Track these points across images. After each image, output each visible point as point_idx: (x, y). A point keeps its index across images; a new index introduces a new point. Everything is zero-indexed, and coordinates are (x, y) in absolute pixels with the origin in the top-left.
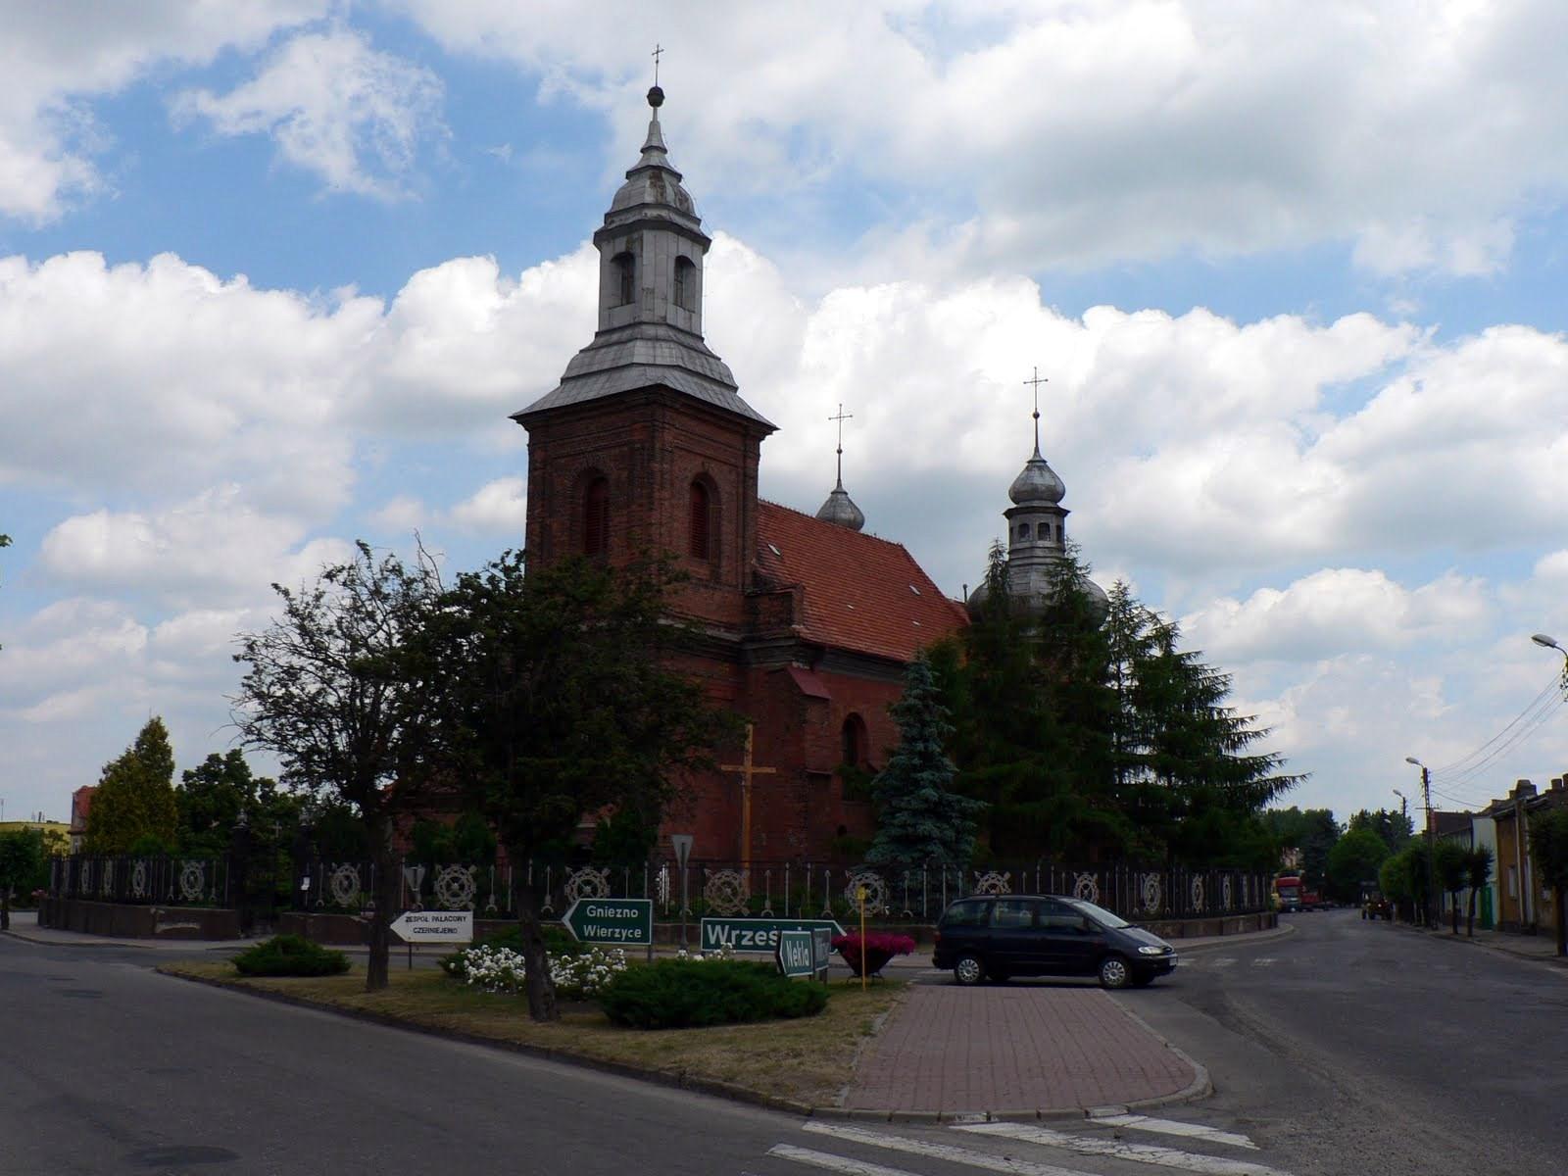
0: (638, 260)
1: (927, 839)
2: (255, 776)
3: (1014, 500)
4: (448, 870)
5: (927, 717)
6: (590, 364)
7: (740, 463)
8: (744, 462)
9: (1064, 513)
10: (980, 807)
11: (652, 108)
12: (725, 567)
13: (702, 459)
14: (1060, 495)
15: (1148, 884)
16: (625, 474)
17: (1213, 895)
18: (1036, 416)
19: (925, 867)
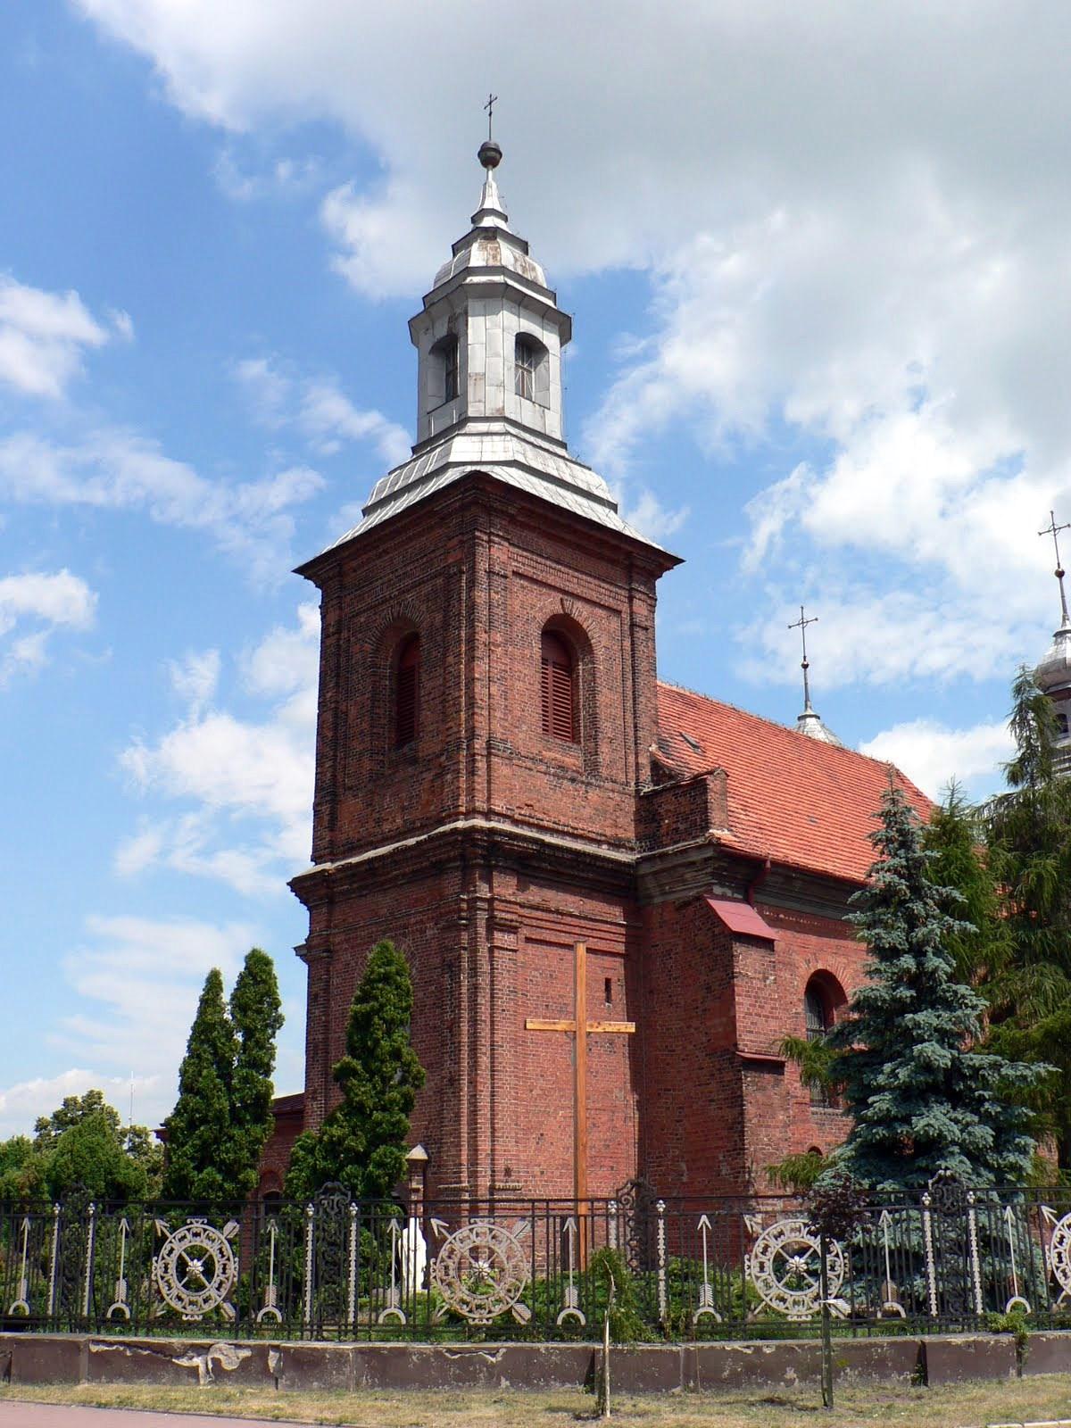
1: (932, 1146)
2: (124, 1124)
5: (918, 907)
7: (625, 608)
8: (631, 607)
10: (1038, 1074)
12: (605, 753)
16: (439, 617)
19: (927, 1199)
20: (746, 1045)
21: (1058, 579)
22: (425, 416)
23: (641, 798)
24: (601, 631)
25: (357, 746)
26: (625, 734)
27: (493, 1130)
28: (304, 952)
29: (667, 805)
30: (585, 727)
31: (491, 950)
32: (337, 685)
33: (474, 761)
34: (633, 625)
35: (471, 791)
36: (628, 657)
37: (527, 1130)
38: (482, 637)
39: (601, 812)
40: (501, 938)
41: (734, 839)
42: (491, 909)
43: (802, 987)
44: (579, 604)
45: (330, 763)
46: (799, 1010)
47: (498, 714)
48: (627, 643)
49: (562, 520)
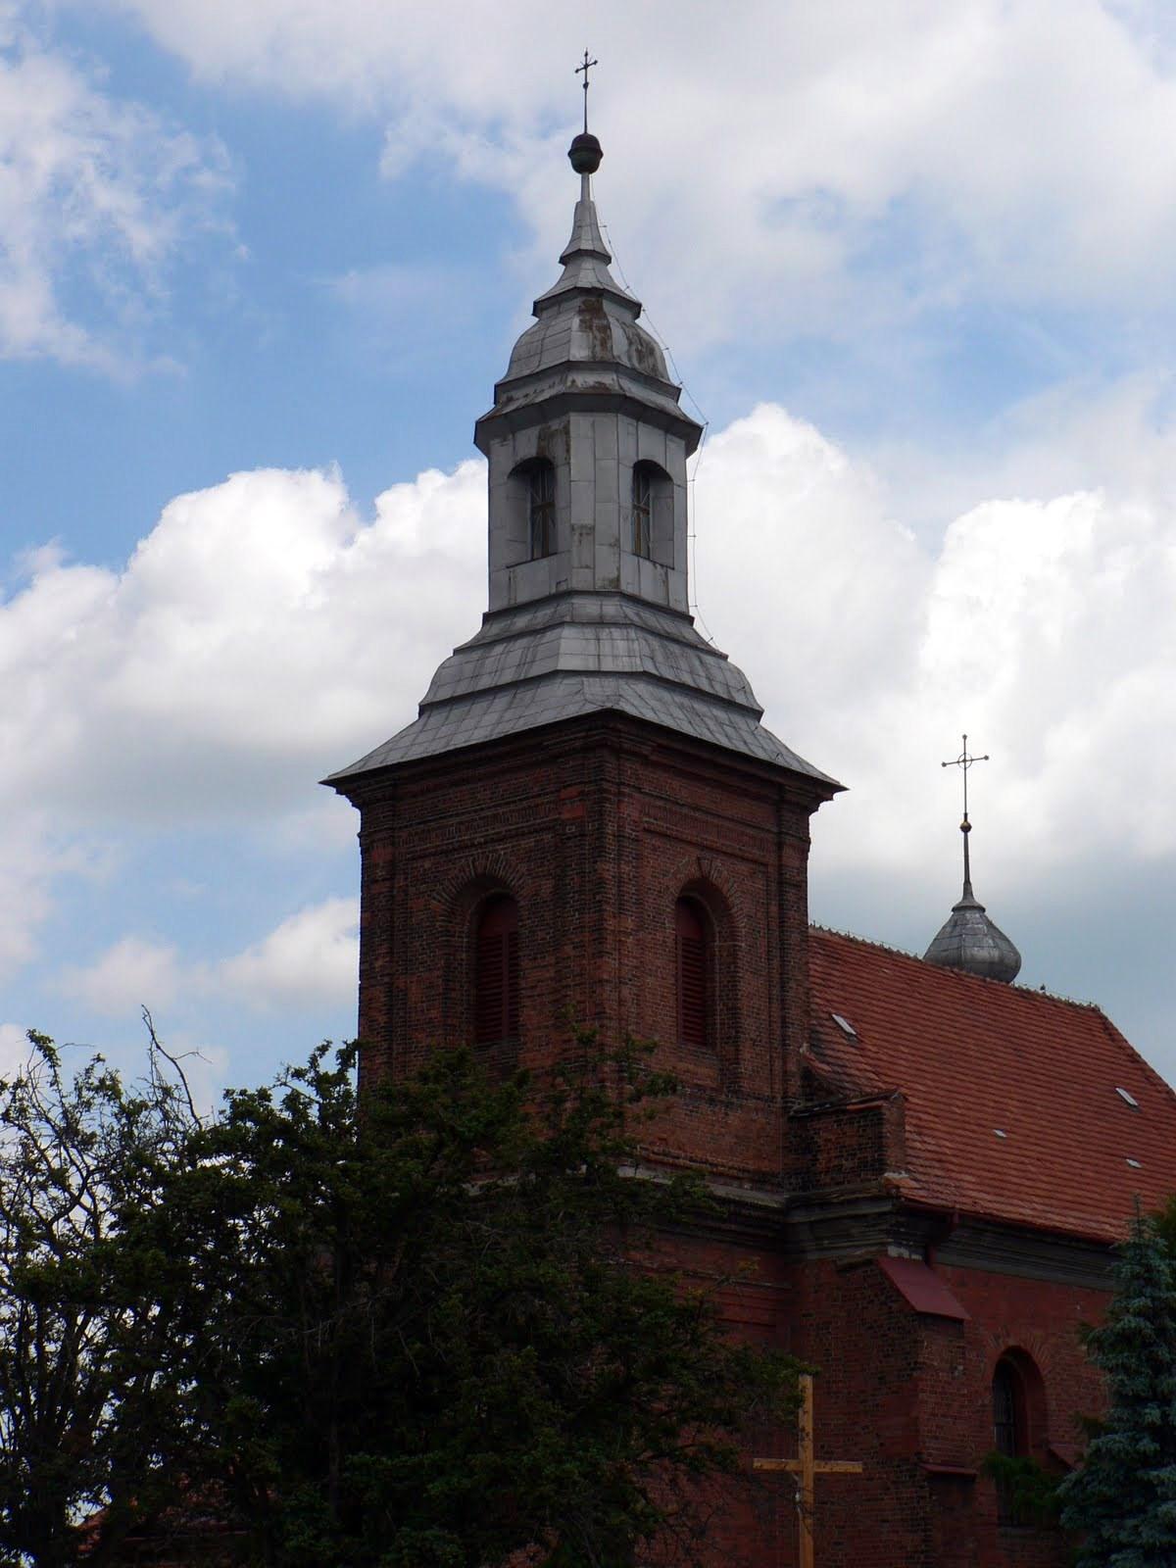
0: (561, 472)
6: (476, 677)
7: (772, 859)
8: (780, 857)
12: (749, 1060)
13: (696, 852)
16: (547, 886)
20: (930, 1455)
23: (791, 1119)
30: (722, 1024)
32: (391, 952)
36: (774, 926)
38: (610, 924)
41: (914, 1184)
43: (990, 1372)
45: (384, 1059)
46: (986, 1402)
49: (705, 755)
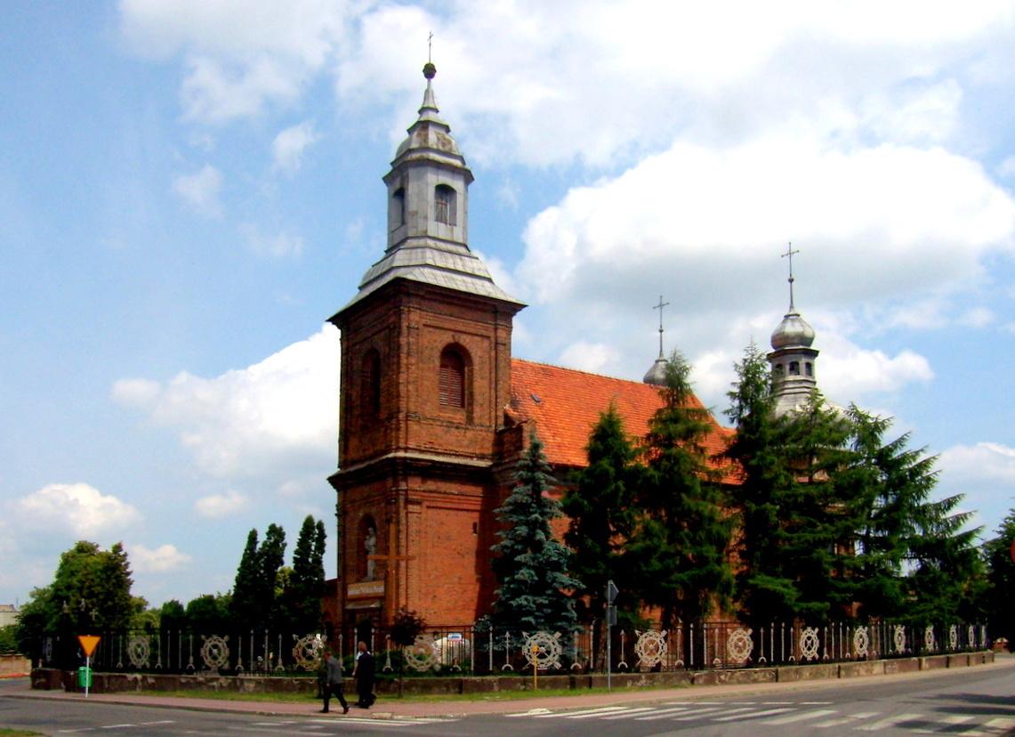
3: (774, 347)
4: (210, 639)
6: (410, 260)
7: (492, 334)
9: (814, 354)
11: (426, 80)
12: (477, 411)
13: (452, 333)
14: (810, 341)
15: (804, 636)
17: (963, 639)
18: (791, 281)
21: (789, 284)
22: (391, 233)
24: (478, 350)
25: (356, 413)
26: (490, 401)
27: (407, 594)
28: (892, 355)
29: (507, 438)
31: (407, 513)
33: (399, 424)
34: (496, 343)
35: (397, 438)
36: (493, 360)
37: (427, 594)
39: (473, 442)
40: (411, 508)
42: (407, 494)
44: (464, 336)
47: (413, 400)
48: (493, 353)
